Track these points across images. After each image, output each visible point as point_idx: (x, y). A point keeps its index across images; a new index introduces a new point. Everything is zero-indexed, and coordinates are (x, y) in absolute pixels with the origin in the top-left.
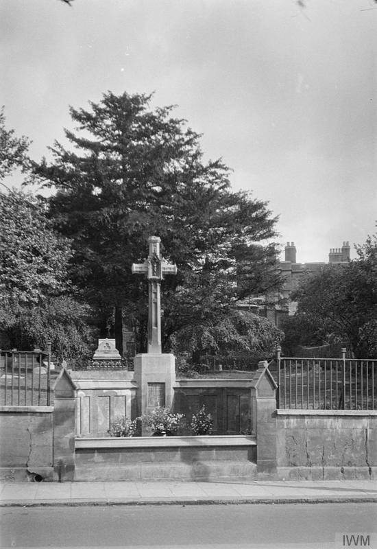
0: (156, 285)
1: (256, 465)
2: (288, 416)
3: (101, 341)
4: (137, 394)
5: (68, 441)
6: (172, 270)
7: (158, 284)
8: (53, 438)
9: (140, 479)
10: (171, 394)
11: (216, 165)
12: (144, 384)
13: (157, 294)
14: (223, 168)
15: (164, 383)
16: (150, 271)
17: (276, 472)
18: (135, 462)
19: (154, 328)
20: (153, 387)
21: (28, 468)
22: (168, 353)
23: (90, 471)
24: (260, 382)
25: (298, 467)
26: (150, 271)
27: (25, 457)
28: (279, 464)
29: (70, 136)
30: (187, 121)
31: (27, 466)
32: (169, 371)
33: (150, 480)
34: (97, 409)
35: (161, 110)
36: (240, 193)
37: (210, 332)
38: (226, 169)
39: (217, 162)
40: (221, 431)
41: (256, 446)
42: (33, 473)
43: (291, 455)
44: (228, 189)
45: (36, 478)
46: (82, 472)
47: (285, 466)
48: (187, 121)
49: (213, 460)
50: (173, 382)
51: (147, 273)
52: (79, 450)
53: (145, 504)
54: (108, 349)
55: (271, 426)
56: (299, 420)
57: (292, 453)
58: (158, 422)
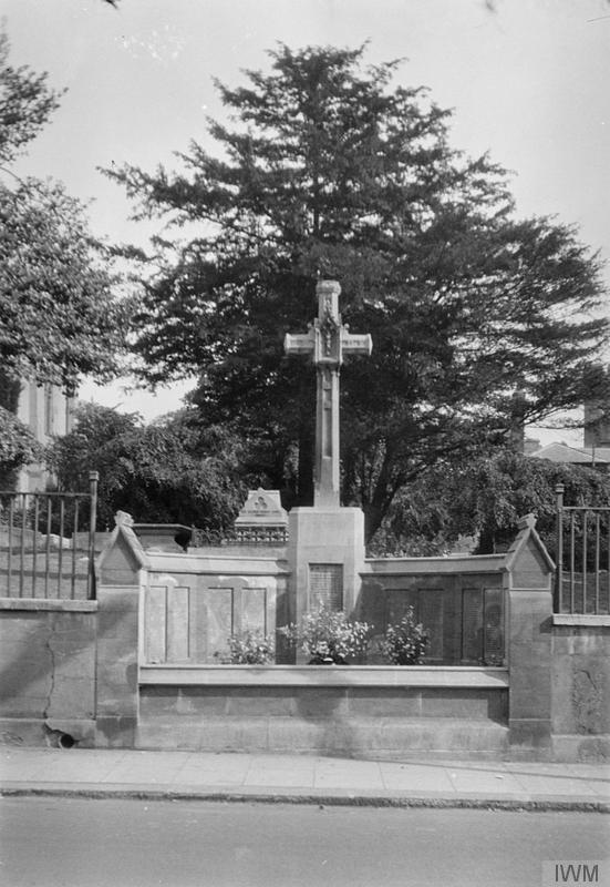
0: (331, 376)
1: (506, 729)
2: (578, 629)
3: (251, 494)
4: (288, 585)
5: (124, 670)
6: (362, 346)
7: (334, 373)
8: (96, 663)
9: (267, 750)
10: (354, 586)
11: (479, 166)
12: (302, 568)
13: (331, 394)
14: (496, 172)
15: (341, 565)
16: (319, 348)
17: (551, 745)
18: (258, 716)
19: (325, 457)
20: (321, 574)
21: (47, 721)
22: (341, 500)
23: (166, 731)
24: (517, 557)
25: (599, 737)
26: (319, 348)
27: (43, 698)
28: (557, 730)
29: (219, 133)
30: (430, 90)
31: (45, 716)
32: (350, 540)
33: (285, 753)
34: (206, 613)
35: (378, 70)
36: (534, 221)
37: (508, 499)
38: (502, 172)
39: (482, 160)
40: (451, 658)
41: (506, 689)
42: (57, 731)
43: (584, 712)
44: (509, 217)
45: (62, 741)
46: (152, 732)
47: (569, 733)
48: (430, 90)
49: (417, 715)
50: (359, 563)
51: (313, 350)
52: (145, 688)
53: (243, 800)
54: (262, 508)
55: (541, 649)
56: (601, 638)
57: (586, 706)
58: (316, 638)
